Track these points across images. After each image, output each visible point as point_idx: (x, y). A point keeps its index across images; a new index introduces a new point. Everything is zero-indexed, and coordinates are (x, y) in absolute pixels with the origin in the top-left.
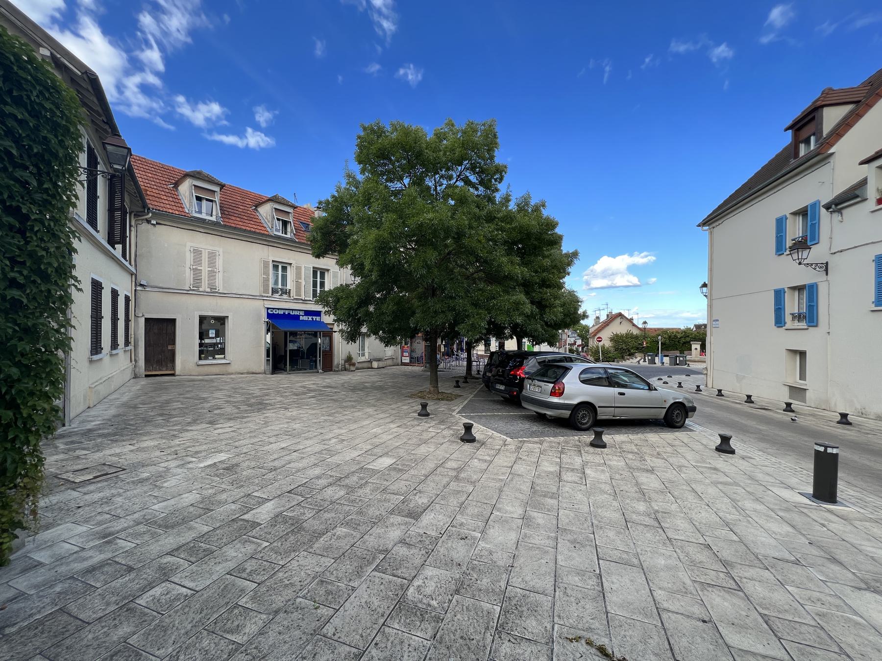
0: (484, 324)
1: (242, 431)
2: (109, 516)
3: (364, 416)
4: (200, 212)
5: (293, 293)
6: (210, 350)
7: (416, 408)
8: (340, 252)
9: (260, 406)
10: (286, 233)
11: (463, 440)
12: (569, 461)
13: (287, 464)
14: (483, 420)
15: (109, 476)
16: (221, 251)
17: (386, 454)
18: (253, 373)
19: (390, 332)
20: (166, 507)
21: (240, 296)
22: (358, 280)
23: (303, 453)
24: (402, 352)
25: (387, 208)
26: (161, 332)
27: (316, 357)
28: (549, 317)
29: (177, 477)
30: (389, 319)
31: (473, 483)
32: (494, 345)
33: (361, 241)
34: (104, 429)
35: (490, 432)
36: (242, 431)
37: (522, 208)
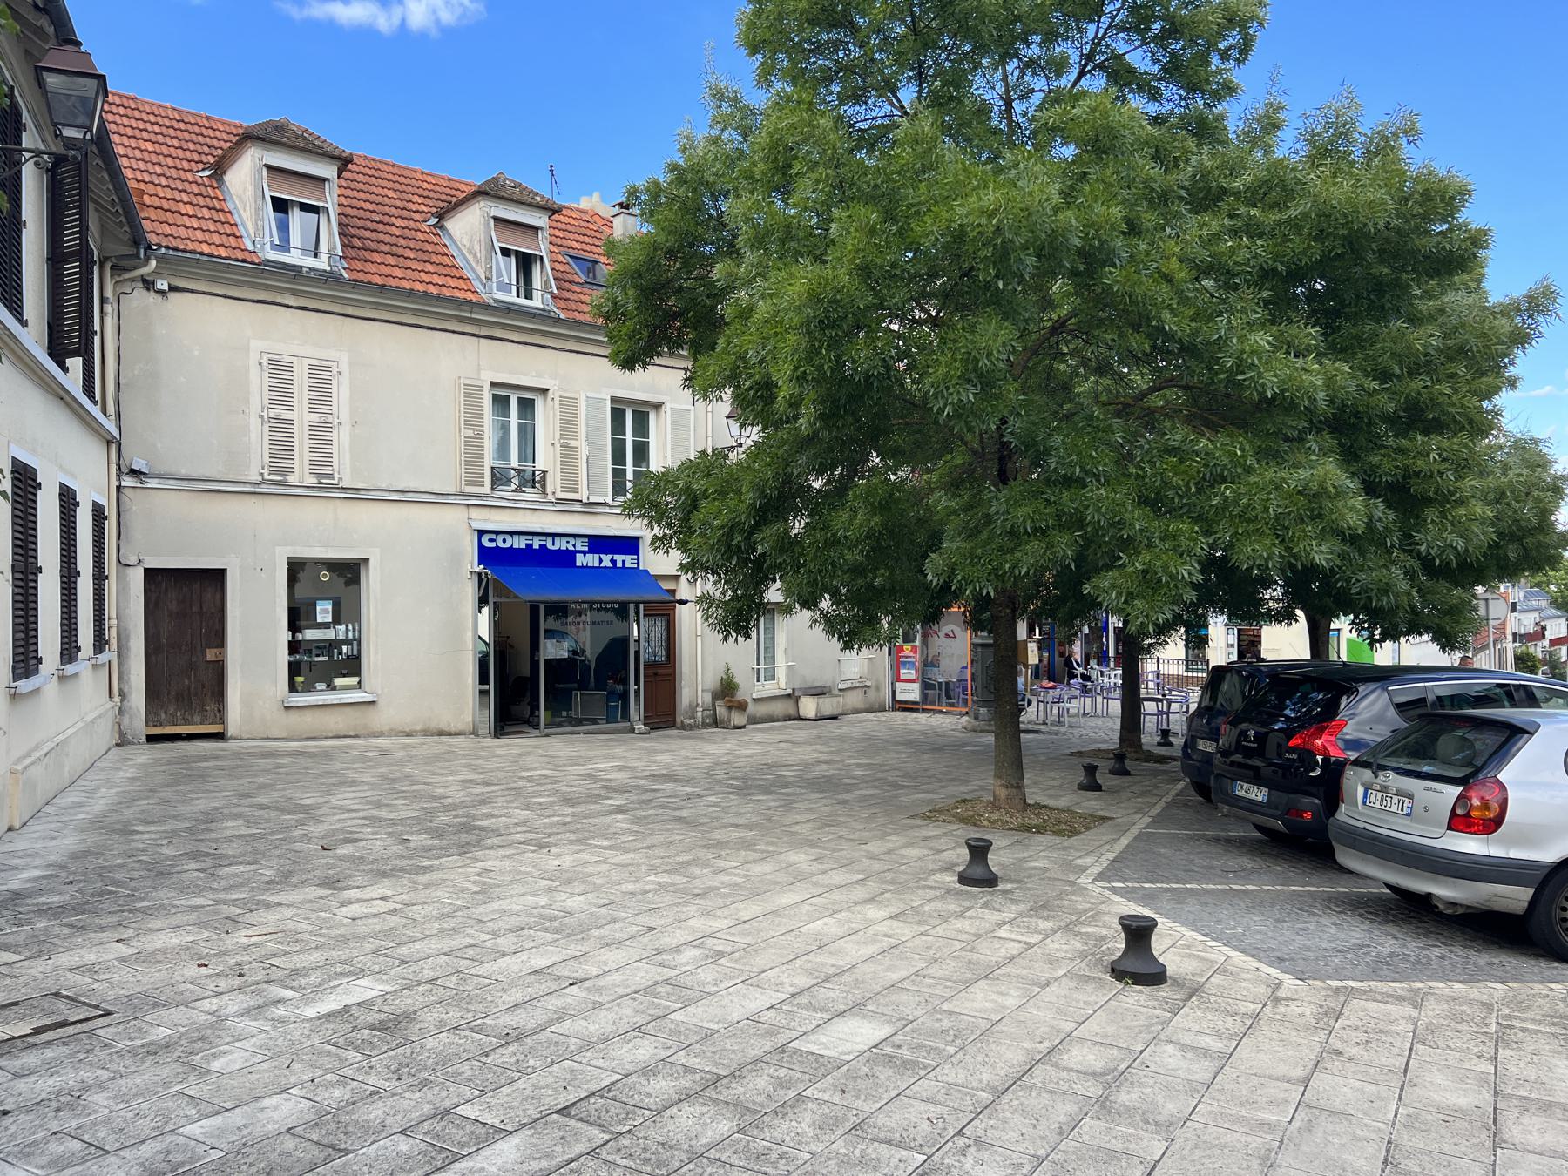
0: (1188, 571)
1: (418, 912)
2: (77, 1145)
3: (781, 877)
4: (285, 246)
5: (554, 484)
6: (320, 662)
7: (949, 856)
8: (697, 350)
9: (465, 837)
10: (528, 296)
11: (1118, 973)
12: (1531, 1073)
13: (552, 1022)
14: (1192, 906)
15: (71, 1030)
16: (345, 358)
17: (857, 1008)
18: (441, 733)
19: (855, 599)
20: (221, 1132)
21: (398, 497)
22: (754, 434)
23: (598, 990)
24: (897, 666)
25: (843, 191)
26: (188, 605)
27: (625, 682)
28: (1436, 538)
29: (246, 1044)
30: (853, 556)
31: (1165, 1128)
32: (1221, 642)
33: (763, 307)
34: (51, 892)
35: (1219, 952)
36: (418, 912)
37: (1324, 151)
